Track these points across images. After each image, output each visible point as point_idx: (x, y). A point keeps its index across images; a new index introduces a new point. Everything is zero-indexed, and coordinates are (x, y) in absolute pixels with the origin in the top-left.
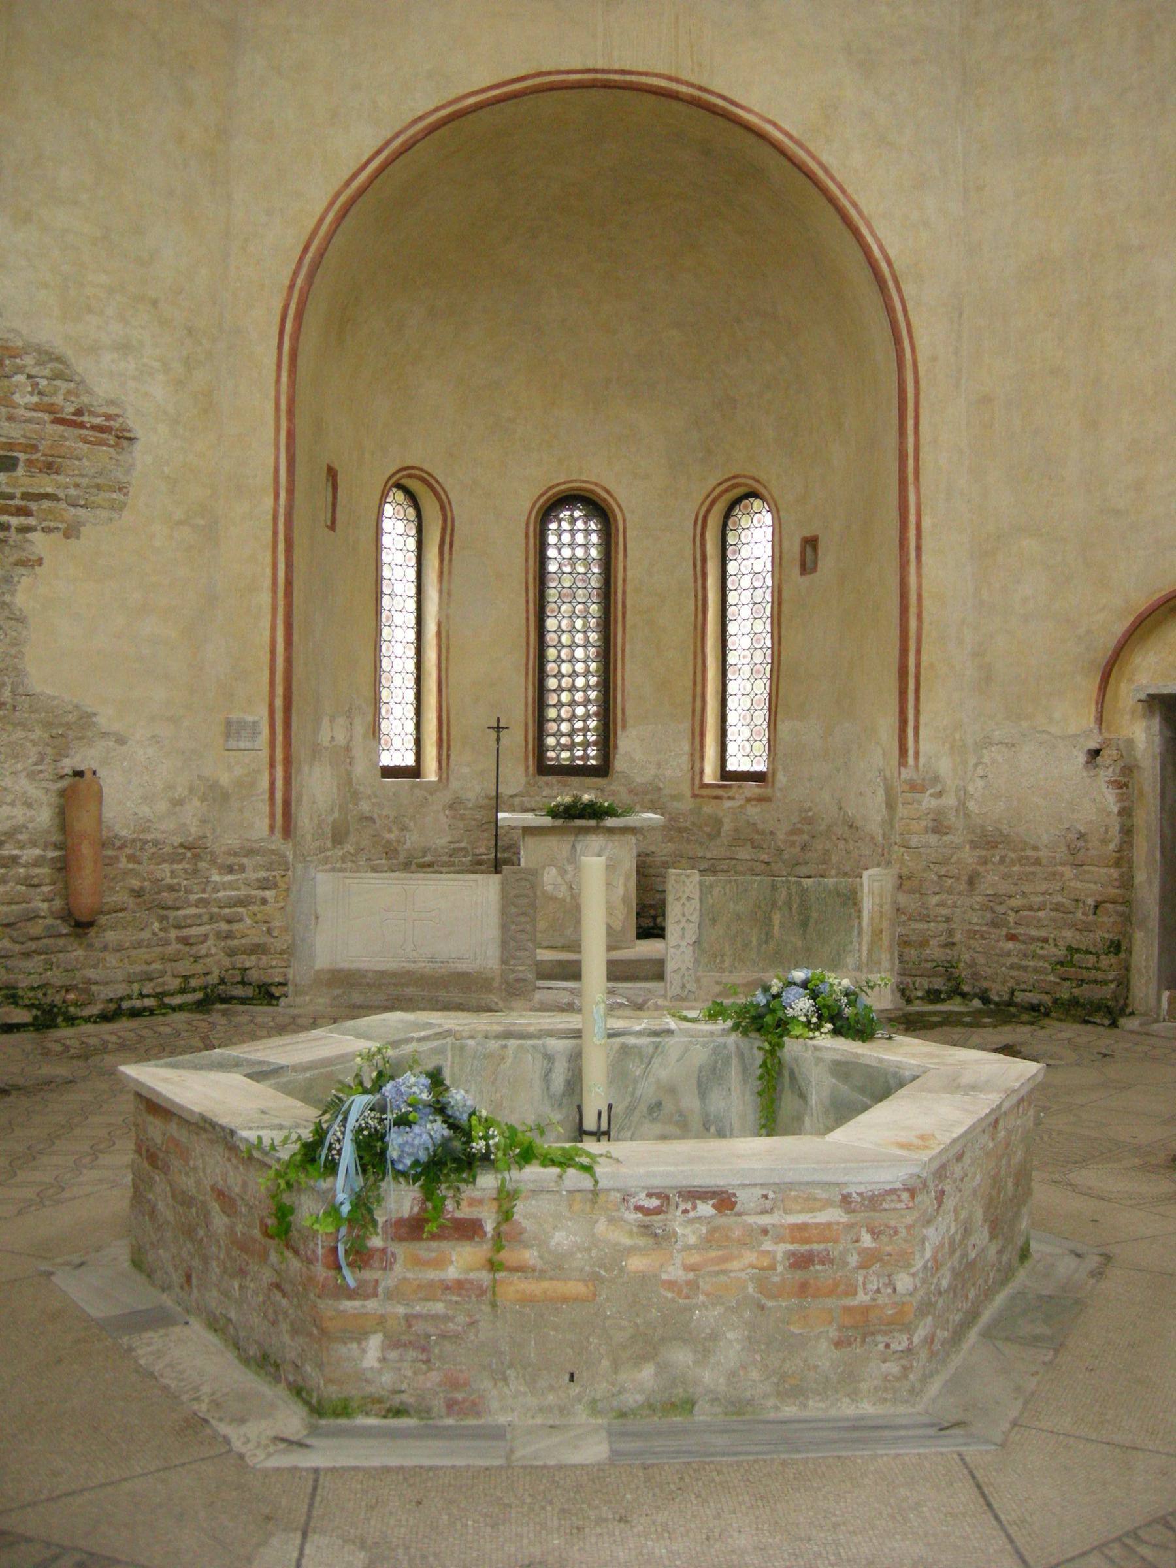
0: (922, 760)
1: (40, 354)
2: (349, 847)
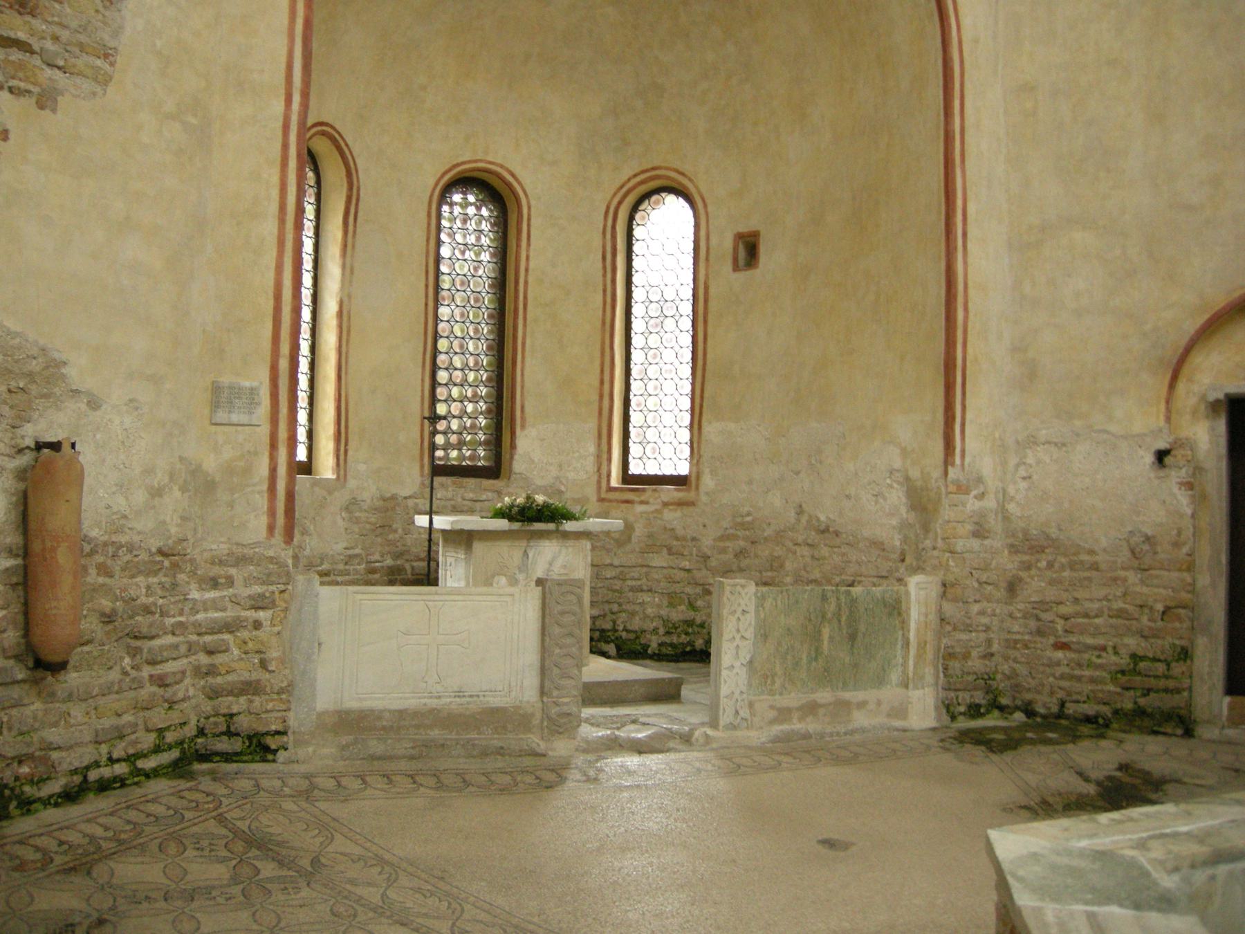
0: (967, 460)
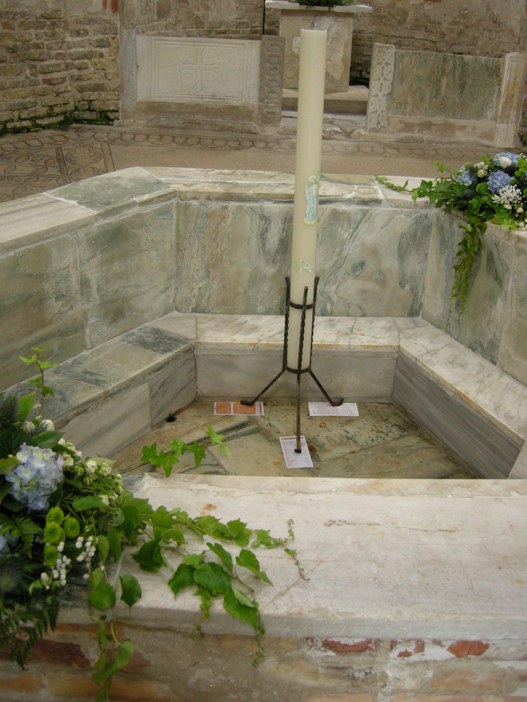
2: (171, 20)
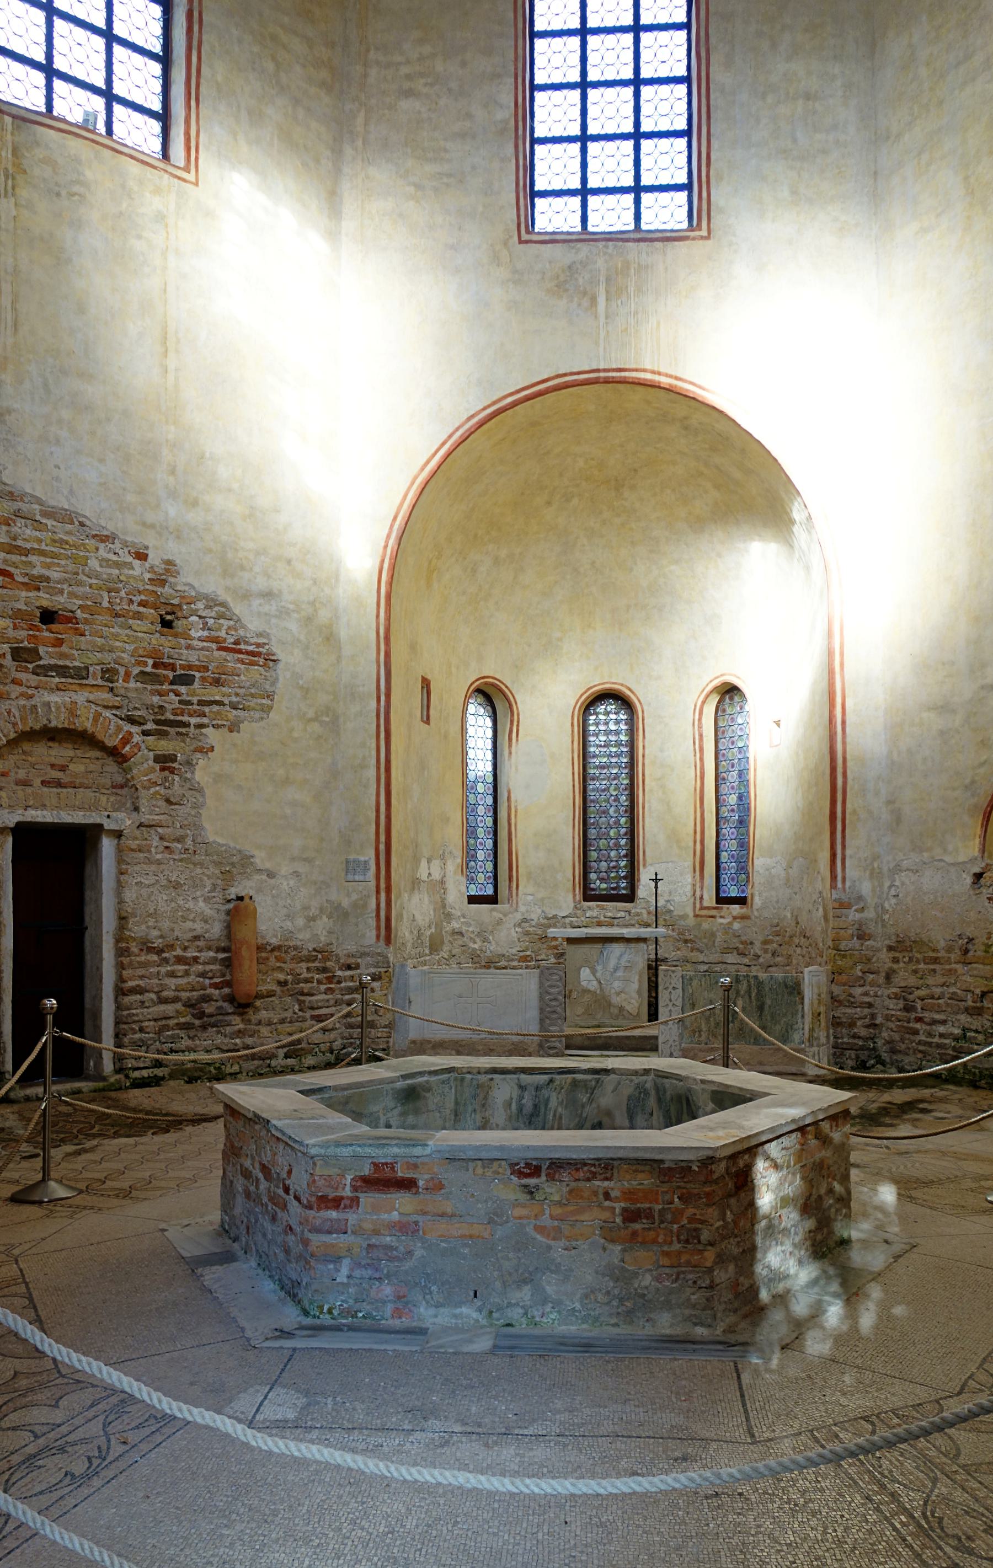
0: (848, 884)
1: (207, 601)
